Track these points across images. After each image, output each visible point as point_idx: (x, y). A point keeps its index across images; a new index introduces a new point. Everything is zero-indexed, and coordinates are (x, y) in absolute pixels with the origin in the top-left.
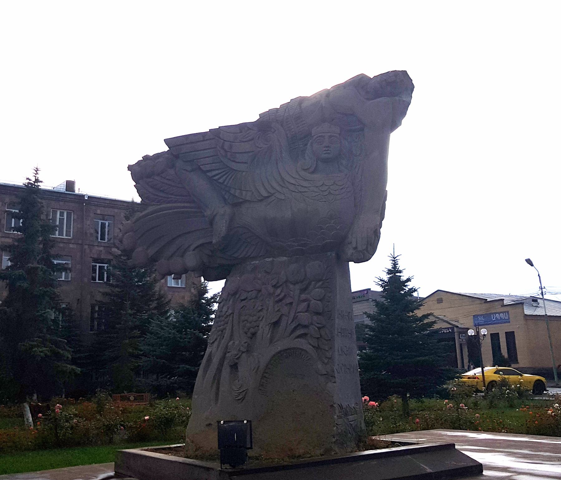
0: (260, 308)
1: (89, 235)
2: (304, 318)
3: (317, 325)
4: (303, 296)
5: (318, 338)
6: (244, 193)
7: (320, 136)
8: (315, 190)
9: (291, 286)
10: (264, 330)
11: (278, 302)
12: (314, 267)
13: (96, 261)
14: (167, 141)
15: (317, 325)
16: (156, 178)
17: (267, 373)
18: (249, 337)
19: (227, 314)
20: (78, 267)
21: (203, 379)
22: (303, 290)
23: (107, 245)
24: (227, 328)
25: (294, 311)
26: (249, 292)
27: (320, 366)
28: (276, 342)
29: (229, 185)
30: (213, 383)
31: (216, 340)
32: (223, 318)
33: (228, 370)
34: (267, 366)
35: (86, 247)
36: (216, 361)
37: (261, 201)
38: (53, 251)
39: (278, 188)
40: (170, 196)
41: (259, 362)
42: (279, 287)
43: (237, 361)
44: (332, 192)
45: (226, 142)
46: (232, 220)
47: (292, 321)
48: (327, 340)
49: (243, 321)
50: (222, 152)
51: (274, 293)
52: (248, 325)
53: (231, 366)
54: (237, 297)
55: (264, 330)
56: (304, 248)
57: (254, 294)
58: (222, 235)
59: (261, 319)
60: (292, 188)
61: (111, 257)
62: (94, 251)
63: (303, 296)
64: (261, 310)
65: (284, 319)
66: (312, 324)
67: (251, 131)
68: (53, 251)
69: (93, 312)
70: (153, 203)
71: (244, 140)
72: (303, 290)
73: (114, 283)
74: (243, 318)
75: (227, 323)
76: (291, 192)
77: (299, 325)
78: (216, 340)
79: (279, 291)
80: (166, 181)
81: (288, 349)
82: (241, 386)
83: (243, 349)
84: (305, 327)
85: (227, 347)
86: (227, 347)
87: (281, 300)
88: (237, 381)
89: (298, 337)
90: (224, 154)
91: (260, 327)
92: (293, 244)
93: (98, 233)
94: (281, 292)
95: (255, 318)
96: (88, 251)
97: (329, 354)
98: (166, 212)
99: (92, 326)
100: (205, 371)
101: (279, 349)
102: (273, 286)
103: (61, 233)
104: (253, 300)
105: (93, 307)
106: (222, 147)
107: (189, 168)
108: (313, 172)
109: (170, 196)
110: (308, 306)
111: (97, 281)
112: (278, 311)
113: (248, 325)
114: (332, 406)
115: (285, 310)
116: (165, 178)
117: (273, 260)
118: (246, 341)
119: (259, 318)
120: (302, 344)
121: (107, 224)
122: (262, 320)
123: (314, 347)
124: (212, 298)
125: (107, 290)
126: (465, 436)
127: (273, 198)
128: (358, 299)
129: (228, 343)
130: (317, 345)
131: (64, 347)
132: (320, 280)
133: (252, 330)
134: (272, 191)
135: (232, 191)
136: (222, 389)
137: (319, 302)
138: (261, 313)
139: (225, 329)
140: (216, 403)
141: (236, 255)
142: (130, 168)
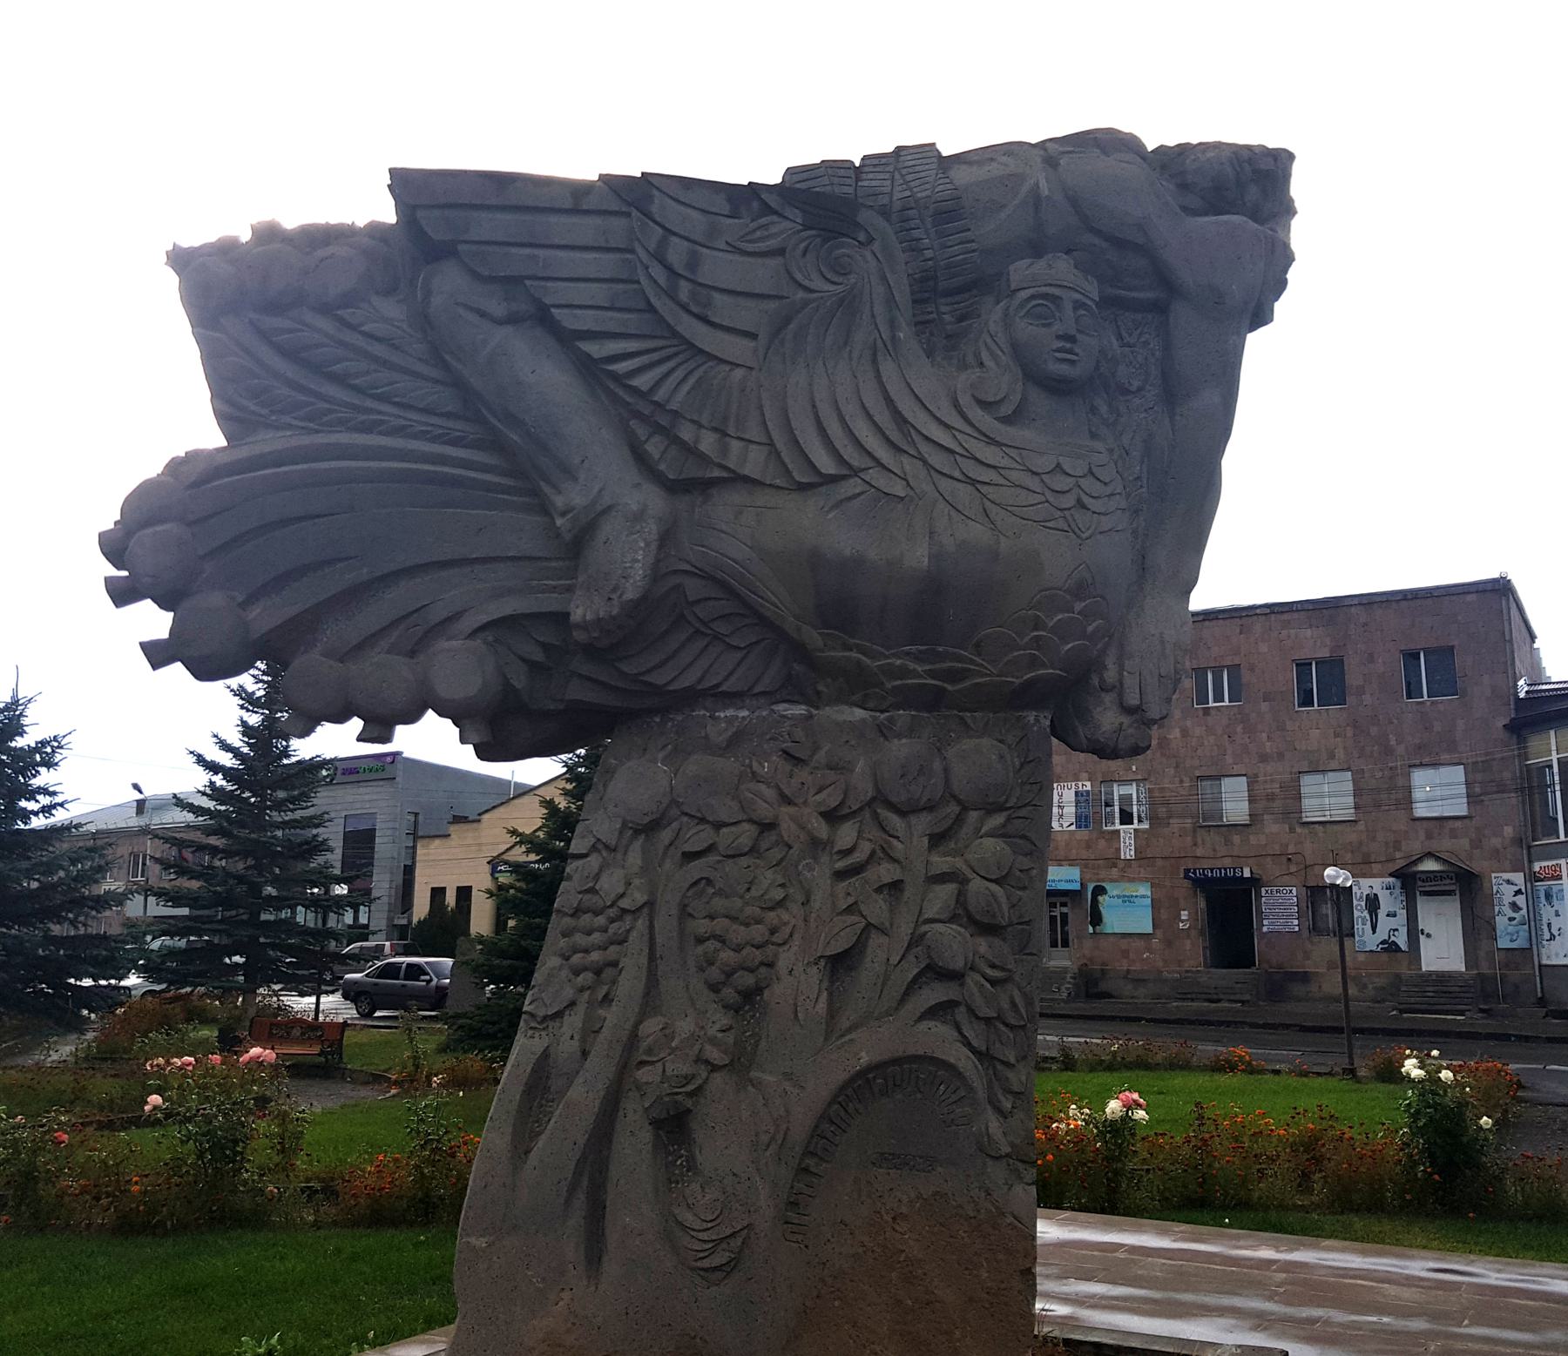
2: (954, 943)
3: (989, 972)
6: (735, 445)
7: (1045, 296)
8: (1033, 483)
9: (895, 821)
11: (840, 875)
12: (978, 756)
14: (404, 183)
15: (989, 972)
16: (309, 317)
17: (813, 1154)
18: (726, 1007)
22: (937, 840)
26: (718, 826)
27: (995, 1125)
28: (849, 1030)
29: (673, 406)
30: (572, 1189)
32: (601, 920)
37: (802, 488)
39: (883, 453)
40: (369, 403)
42: (846, 818)
43: (689, 1103)
44: (1086, 500)
45: (674, 239)
46: (666, 538)
49: (700, 940)
50: (657, 272)
51: (830, 842)
52: (726, 955)
53: (656, 1124)
55: (797, 983)
56: (949, 687)
58: (631, 594)
59: (777, 938)
60: (937, 459)
64: (780, 904)
65: (875, 940)
67: (775, 218)
70: (287, 419)
71: (750, 247)
72: (937, 840)
76: (922, 477)
78: (572, 1004)
80: (360, 341)
83: (714, 1054)
84: (956, 976)
85: (634, 1037)
86: (634, 1037)
87: (856, 870)
89: (933, 1012)
90: (662, 281)
92: (912, 666)
95: (758, 932)
98: (333, 464)
101: (865, 1059)
102: (821, 814)
106: (659, 257)
107: (498, 308)
108: (1007, 420)
109: (369, 403)
110: (961, 898)
113: (726, 955)
115: (877, 908)
116: (353, 328)
117: (811, 716)
119: (773, 932)
124: (33, 750)
127: (852, 486)
128: (374, 776)
132: (1001, 808)
133: (748, 980)
134: (856, 460)
135: (686, 433)
137: (994, 887)
141: (659, 679)
142: (180, 259)
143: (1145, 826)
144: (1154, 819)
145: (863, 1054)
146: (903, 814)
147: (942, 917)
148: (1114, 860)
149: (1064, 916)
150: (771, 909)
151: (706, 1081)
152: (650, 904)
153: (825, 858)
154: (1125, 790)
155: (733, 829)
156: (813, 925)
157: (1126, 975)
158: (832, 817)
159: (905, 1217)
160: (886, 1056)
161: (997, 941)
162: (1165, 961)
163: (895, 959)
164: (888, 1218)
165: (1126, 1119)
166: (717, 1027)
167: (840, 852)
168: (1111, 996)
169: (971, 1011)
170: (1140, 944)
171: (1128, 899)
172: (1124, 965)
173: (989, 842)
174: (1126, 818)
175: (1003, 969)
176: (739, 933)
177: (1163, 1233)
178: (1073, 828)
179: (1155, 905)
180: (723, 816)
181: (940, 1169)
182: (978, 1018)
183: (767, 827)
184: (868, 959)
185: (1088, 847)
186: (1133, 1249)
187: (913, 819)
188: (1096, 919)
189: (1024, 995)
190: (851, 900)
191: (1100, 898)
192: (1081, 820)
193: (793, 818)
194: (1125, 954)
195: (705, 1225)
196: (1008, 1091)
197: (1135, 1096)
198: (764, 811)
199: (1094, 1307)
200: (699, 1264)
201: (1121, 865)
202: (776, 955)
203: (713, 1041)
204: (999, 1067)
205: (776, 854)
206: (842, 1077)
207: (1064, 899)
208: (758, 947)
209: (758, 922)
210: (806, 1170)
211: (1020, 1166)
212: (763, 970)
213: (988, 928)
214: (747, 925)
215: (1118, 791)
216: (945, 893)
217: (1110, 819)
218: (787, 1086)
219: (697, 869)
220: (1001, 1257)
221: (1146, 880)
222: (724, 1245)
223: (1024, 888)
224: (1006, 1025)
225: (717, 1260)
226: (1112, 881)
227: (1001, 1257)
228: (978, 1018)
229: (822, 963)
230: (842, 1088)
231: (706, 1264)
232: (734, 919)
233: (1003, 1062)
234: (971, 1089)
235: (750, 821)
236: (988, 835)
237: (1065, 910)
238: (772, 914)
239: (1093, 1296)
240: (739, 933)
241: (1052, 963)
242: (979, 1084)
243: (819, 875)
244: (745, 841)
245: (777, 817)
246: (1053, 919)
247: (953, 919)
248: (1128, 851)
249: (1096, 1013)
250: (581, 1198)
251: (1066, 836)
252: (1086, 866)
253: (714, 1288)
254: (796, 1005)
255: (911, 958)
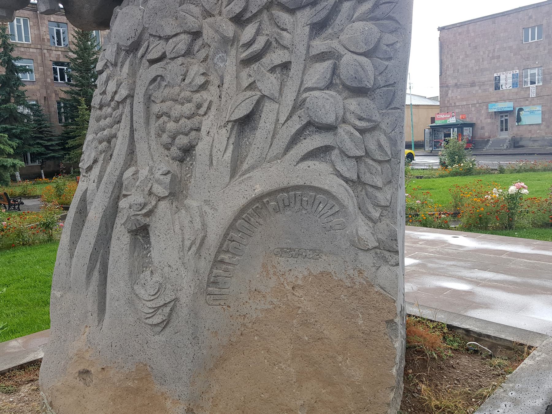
0: (201, 80)
1: (46, 41)
2: (327, 105)
4: (320, 45)
5: (358, 159)
10: (214, 139)
13: (57, 63)
19: (117, 98)
20: (41, 69)
21: (71, 257)
22: (318, 28)
23: (63, 50)
24: (120, 135)
25: (295, 88)
26: (167, 39)
31: (95, 161)
33: (126, 238)
34: (226, 235)
35: (45, 51)
36: (95, 215)
38: (14, 54)
41: (204, 225)
42: (249, 21)
43: (144, 221)
47: (290, 117)
48: (380, 162)
49: (158, 117)
51: (235, 39)
52: (171, 126)
54: (140, 54)
55: (214, 139)
57: (183, 42)
59: (202, 111)
61: (68, 61)
62: (52, 55)
63: (320, 45)
64: (203, 87)
65: (268, 107)
66: (344, 121)
68: (14, 54)
69: (59, 108)
72: (318, 28)
73: (75, 83)
74: (156, 108)
75: (119, 122)
77: (309, 124)
78: (95, 161)
79: (249, 32)
81: (285, 190)
82: (160, 290)
84: (330, 128)
85: (119, 184)
86: (119, 184)
88: (148, 273)
91: (204, 129)
93: (54, 38)
94: (258, 33)
95: (188, 108)
96: (47, 55)
97: (382, 197)
99: (60, 120)
100: (74, 243)
101: (259, 189)
102: (231, 19)
103: (20, 38)
104: (180, 60)
105: (59, 103)
110: (335, 70)
111: (59, 81)
112: (251, 86)
114: (390, 322)
115: (269, 83)
118: (165, 169)
119: (199, 106)
120: (319, 173)
121: (61, 31)
122: (206, 114)
123: (347, 180)
125: (68, 88)
126: (443, 242)
129: (122, 174)
130: (355, 177)
131: (6, 142)
133: (182, 140)
136: (111, 290)
138: (204, 94)
139: (115, 136)
140: (101, 320)
143: (541, 84)
144: (544, 80)
145: (258, 186)
146: (292, 11)
147: (320, 85)
148: (527, 98)
149: (506, 120)
150: (197, 91)
151: (155, 206)
152: (131, 96)
153: (233, 52)
154: (533, 71)
155: (174, 39)
156: (223, 99)
157: (531, 139)
158: (239, 20)
159: (299, 287)
160: (275, 187)
161: (365, 101)
162: (546, 133)
163: (282, 119)
164: (289, 288)
165: (518, 193)
166: (160, 172)
167: (244, 45)
168: (524, 147)
169: (344, 154)
170: (536, 127)
171: (532, 112)
172: (529, 135)
173: (359, 25)
174: (533, 83)
175: (369, 120)
176: (177, 110)
177: (527, 245)
178: (511, 88)
179: (543, 113)
180: (168, 31)
181: (324, 257)
182: (349, 157)
183: (197, 34)
184: (262, 121)
185: (517, 94)
186: (512, 254)
187: (299, 14)
188: (519, 120)
189: (390, 139)
190: (251, 80)
191: (521, 113)
192: (514, 85)
193: (211, 26)
194: (530, 131)
195: (153, 298)
196: (377, 205)
197: (523, 184)
198: (192, 23)
199: (484, 286)
200: (147, 321)
201: (530, 99)
202: (201, 123)
203: (158, 181)
204: (370, 190)
205: (202, 54)
206: (243, 202)
207: (506, 114)
208: (189, 118)
209: (189, 101)
210: (222, 262)
211: (387, 254)
212: (193, 133)
213: (360, 91)
214: (182, 104)
215: (530, 72)
216: (321, 70)
217: (526, 82)
218: (206, 208)
219: (156, 70)
220: (372, 312)
221: (540, 104)
222: (160, 311)
223: (390, 59)
224: (373, 160)
225: (157, 319)
226: (526, 106)
227: (372, 312)
228: (349, 157)
229: (230, 125)
230: (243, 210)
231: (150, 321)
232: (175, 101)
233: (372, 186)
234: (342, 206)
235: (185, 32)
236: (359, 19)
237: (506, 118)
238: (198, 95)
239: (485, 279)
240: (177, 110)
241: (501, 137)
242: (351, 204)
243: (229, 64)
244: (182, 47)
245: (201, 27)
246: (502, 122)
247: (330, 86)
248: (533, 93)
249: (517, 153)
250: (96, 274)
251: (508, 91)
252: (516, 101)
253: (156, 336)
254: (211, 155)
255: (295, 117)
